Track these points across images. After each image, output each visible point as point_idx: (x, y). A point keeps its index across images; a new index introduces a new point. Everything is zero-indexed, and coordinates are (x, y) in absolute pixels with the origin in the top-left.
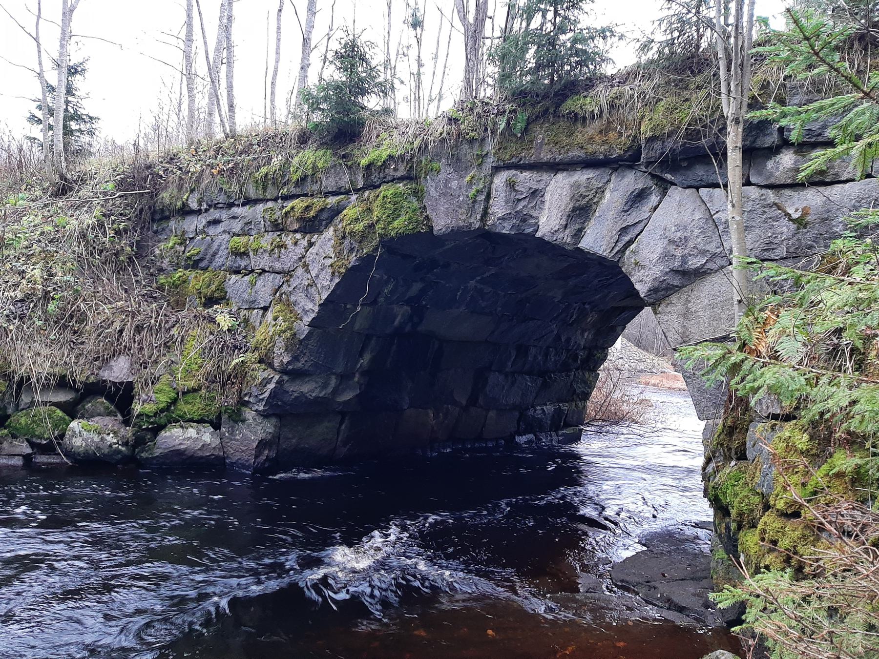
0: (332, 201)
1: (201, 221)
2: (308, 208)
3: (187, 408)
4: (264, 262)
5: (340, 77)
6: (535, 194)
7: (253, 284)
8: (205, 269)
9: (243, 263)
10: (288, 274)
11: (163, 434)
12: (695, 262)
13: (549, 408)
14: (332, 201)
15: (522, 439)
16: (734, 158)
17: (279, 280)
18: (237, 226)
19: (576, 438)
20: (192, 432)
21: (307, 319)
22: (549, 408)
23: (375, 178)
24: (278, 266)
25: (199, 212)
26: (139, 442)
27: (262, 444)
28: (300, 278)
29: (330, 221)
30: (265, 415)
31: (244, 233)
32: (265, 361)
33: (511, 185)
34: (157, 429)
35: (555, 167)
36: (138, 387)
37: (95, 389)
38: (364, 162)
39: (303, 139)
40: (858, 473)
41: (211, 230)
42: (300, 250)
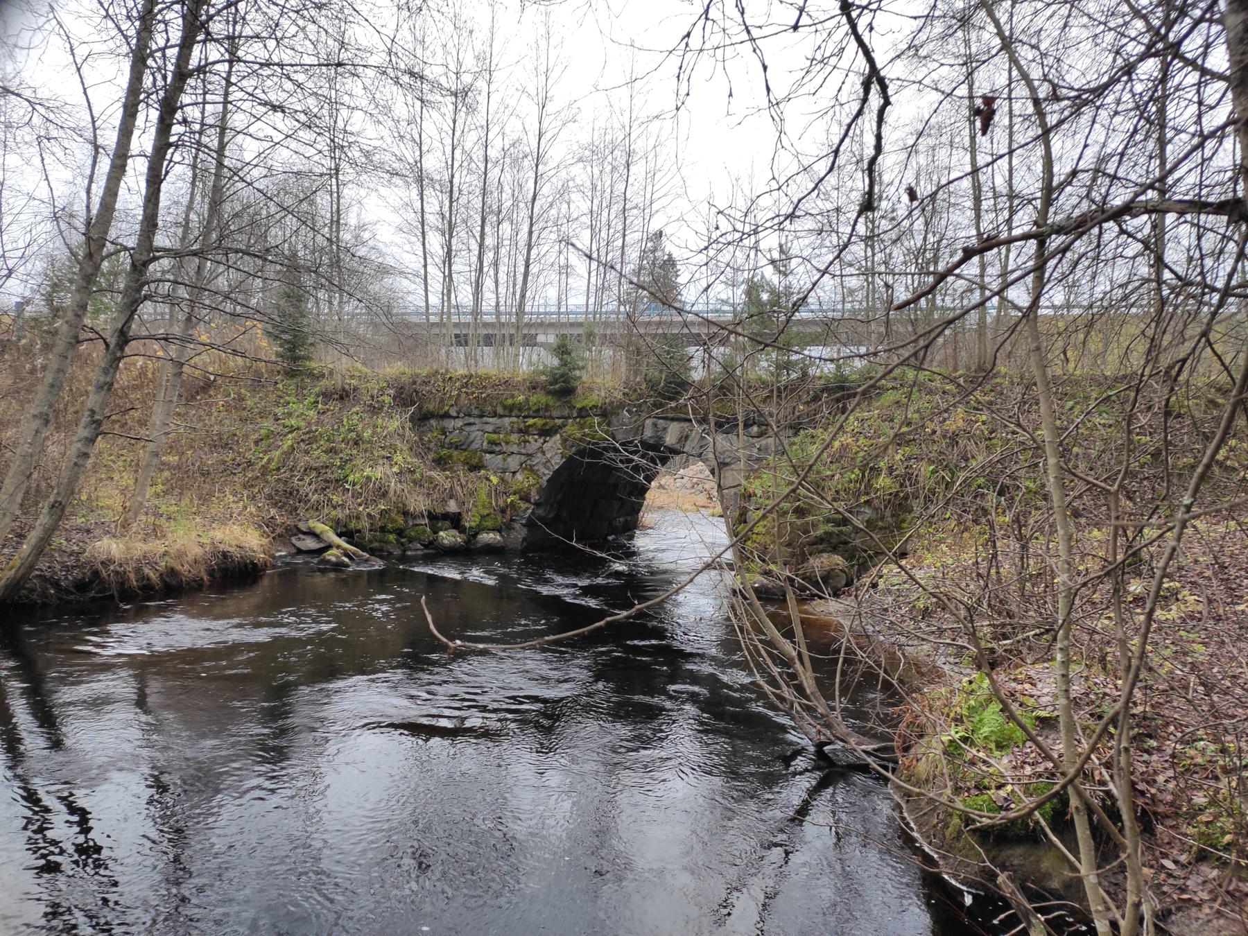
0: (558, 422)
1: (459, 423)
2: (545, 424)
3: (489, 523)
4: (515, 448)
5: (556, 362)
6: (665, 429)
7: (504, 460)
8: (465, 450)
9: (497, 449)
10: (530, 456)
11: (480, 537)
12: (727, 460)
13: (622, 519)
14: (558, 422)
15: (610, 538)
16: (741, 426)
17: (523, 458)
18: (490, 428)
19: (631, 538)
20: (491, 535)
21: (546, 478)
22: (622, 519)
23: (584, 413)
24: (523, 451)
25: (454, 418)
26: (468, 542)
27: (524, 539)
28: (538, 459)
29: (556, 432)
30: (524, 525)
31: (495, 432)
32: (526, 498)
33: (655, 425)
34: (477, 534)
35: (673, 419)
36: (464, 515)
37: (446, 516)
38: (578, 406)
39: (534, 387)
40: (750, 496)
41: (467, 429)
42: (539, 444)
